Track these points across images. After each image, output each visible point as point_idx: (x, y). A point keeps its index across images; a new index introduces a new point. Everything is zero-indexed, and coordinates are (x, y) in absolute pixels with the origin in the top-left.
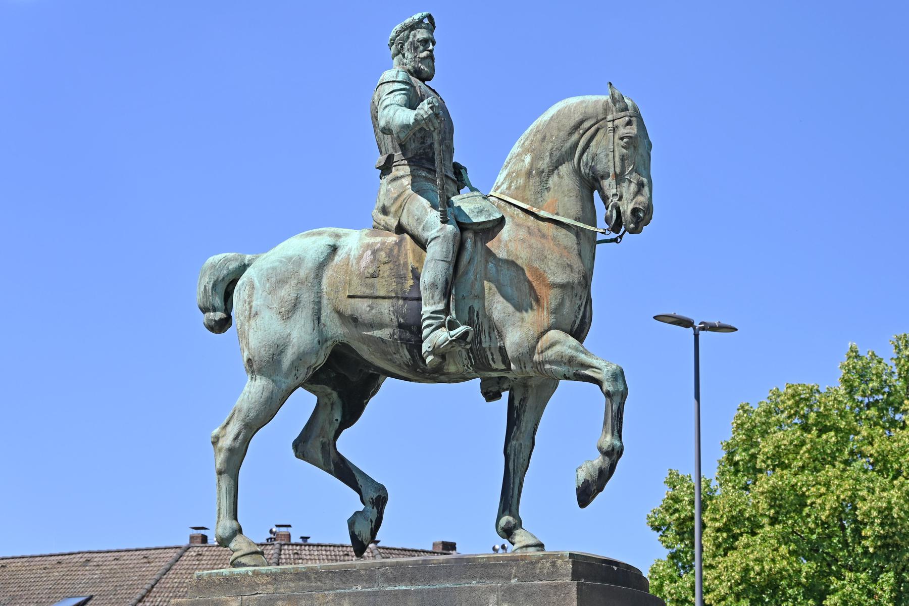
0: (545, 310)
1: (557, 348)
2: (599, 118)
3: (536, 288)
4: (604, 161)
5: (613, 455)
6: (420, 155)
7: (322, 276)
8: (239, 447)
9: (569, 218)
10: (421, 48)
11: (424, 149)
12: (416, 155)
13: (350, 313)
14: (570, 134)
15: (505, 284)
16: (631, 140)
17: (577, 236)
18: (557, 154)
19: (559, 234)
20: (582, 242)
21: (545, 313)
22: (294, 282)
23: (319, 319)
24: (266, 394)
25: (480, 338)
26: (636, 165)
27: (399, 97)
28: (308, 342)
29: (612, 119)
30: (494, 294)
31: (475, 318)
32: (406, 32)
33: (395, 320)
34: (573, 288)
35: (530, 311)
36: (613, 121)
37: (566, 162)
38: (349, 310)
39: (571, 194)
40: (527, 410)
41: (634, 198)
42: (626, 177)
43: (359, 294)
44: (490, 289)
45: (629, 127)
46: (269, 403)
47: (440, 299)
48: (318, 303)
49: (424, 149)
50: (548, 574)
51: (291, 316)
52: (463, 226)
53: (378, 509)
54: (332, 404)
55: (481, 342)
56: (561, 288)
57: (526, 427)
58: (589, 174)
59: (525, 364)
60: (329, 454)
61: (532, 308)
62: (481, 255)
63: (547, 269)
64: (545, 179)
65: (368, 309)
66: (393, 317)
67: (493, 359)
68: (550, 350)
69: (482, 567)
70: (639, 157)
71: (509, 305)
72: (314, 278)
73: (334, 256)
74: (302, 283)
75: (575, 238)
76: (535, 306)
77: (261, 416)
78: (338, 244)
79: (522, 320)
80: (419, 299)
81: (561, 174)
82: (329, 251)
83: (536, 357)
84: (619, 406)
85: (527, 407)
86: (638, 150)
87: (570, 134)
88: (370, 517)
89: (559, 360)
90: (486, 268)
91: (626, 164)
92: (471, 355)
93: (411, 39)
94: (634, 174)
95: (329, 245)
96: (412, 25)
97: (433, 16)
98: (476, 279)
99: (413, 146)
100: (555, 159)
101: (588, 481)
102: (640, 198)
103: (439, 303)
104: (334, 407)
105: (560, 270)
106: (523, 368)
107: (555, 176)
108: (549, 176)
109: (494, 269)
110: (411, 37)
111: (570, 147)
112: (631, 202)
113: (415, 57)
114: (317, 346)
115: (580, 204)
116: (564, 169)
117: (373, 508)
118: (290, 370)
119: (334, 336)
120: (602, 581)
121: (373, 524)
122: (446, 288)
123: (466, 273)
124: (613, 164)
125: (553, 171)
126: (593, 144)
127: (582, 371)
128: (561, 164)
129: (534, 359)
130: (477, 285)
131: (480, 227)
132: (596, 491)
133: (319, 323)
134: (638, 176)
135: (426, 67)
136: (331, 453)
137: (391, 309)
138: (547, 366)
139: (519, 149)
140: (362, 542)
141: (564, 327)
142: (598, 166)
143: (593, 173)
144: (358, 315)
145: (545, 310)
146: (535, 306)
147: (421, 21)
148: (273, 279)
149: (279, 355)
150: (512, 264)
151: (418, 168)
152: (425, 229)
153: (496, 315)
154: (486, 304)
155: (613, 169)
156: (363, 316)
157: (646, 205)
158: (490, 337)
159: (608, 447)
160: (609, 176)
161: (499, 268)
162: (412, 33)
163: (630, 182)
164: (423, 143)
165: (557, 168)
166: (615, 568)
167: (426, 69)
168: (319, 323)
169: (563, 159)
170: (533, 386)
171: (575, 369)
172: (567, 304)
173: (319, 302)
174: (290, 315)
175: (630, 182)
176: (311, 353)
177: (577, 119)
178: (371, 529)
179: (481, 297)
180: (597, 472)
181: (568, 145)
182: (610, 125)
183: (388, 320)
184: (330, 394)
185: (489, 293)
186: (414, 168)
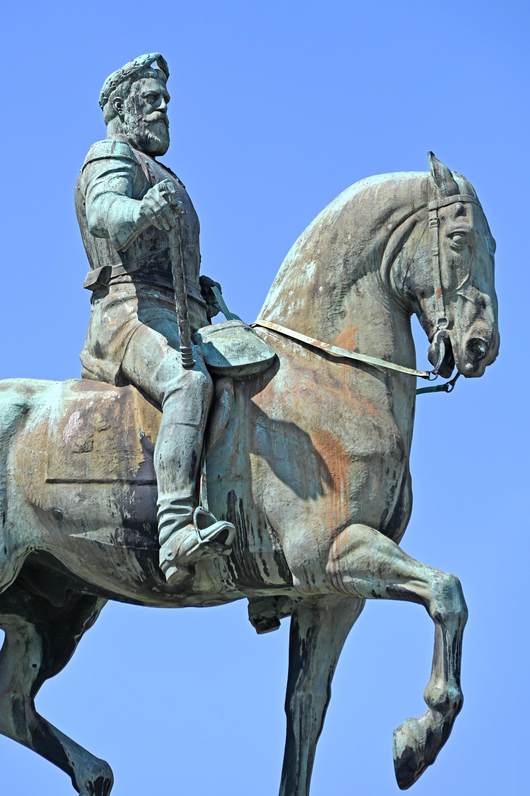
0: (342, 494)
1: (361, 552)
2: (416, 206)
3: (327, 462)
4: (425, 270)
5: (448, 709)
6: (150, 267)
9: (375, 355)
10: (149, 106)
11: (155, 259)
12: (144, 267)
13: (51, 506)
14: (374, 231)
16: (464, 238)
17: (388, 383)
18: (354, 261)
19: (361, 381)
21: (342, 500)
26: (472, 274)
27: (117, 181)
30: (265, 473)
31: (238, 509)
32: (126, 83)
33: (118, 514)
34: (382, 461)
35: (319, 497)
36: (437, 209)
37: (369, 273)
38: (49, 501)
39: (377, 321)
40: (318, 644)
41: (471, 324)
42: (459, 293)
43: (63, 477)
44: (259, 465)
45: (461, 218)
47: (184, 482)
54: (27, 643)
56: (365, 461)
57: (318, 670)
58: (402, 290)
59: (313, 576)
60: (24, 717)
61: (323, 494)
63: (343, 433)
64: (337, 299)
65: (77, 499)
67: (265, 570)
70: (478, 262)
75: (384, 385)
76: (327, 490)
78: (30, 402)
79: (308, 510)
81: (361, 290)
82: (17, 414)
83: (330, 566)
84: (456, 635)
86: (475, 252)
87: (374, 231)
89: (365, 568)
90: (252, 434)
91: (458, 274)
92: (232, 564)
93: (132, 94)
94: (470, 288)
95: (17, 405)
96: (135, 73)
99: (139, 253)
101: (411, 749)
103: (182, 488)
104: (31, 646)
105: (362, 434)
106: (311, 583)
108: (343, 294)
109: (264, 436)
110: (133, 90)
111: (374, 251)
112: (467, 331)
115: (391, 335)
123: (222, 442)
124: (437, 274)
125: (349, 286)
126: (408, 244)
127: (399, 585)
128: (361, 276)
129: (327, 568)
130: (240, 458)
131: (242, 373)
132: (423, 764)
133: (4, 522)
134: (476, 292)
135: (156, 135)
138: (347, 579)
141: (370, 519)
142: (417, 277)
143: (409, 288)
144: (63, 509)
145: (342, 494)
146: (327, 490)
147: (147, 66)
151: (148, 287)
152: (160, 378)
154: (254, 488)
155: (439, 282)
156: (71, 510)
157: (489, 334)
158: (260, 537)
159: (441, 698)
160: (432, 292)
161: (272, 434)
162: (135, 84)
163: (465, 300)
164: (154, 248)
165: (355, 281)
169: (364, 268)
170: (327, 608)
172: (375, 485)
175: (465, 300)
177: (383, 208)
180: (425, 736)
181: (371, 246)
182: (433, 215)
183: (108, 515)
186: (141, 286)
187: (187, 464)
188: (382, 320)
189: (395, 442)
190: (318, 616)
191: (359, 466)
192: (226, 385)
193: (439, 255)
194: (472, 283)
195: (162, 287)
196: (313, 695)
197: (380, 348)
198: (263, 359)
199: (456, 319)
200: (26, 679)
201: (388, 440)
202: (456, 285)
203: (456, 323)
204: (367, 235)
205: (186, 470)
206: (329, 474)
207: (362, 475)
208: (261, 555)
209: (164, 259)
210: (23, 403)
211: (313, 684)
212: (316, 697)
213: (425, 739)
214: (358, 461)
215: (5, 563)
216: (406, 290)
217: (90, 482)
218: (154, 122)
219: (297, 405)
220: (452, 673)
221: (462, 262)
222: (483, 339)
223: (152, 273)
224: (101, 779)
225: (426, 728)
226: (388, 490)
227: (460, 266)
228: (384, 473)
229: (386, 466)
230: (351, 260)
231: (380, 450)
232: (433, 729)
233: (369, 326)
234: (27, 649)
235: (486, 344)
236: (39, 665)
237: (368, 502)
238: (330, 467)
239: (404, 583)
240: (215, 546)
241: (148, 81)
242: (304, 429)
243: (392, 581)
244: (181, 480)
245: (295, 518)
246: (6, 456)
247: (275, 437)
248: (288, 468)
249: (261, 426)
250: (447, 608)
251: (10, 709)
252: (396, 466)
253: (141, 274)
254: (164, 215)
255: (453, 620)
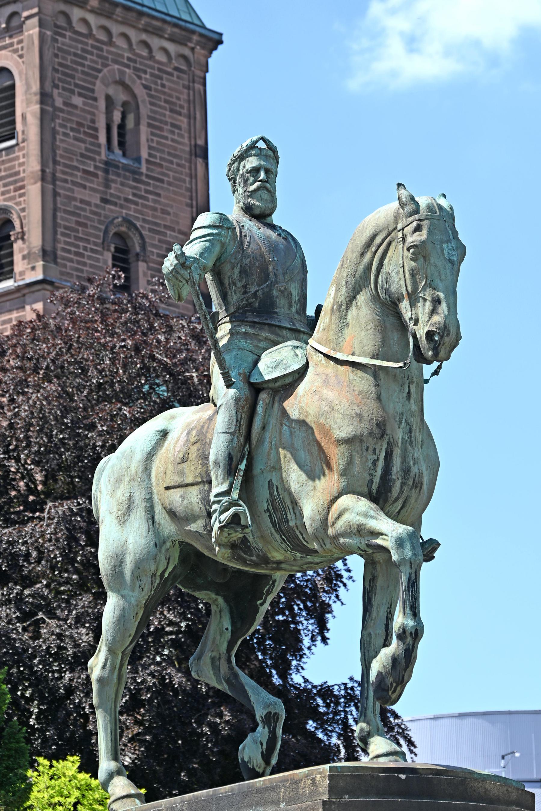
0: (335, 472)
1: (346, 517)
2: (390, 229)
3: (324, 448)
5: (406, 638)
7: (151, 468)
8: (108, 677)
9: (365, 356)
10: (252, 179)
11: (247, 300)
12: (238, 308)
14: (363, 254)
15: (299, 448)
16: (417, 250)
17: (375, 376)
20: (382, 383)
21: (336, 477)
22: (127, 479)
23: (153, 518)
24: (117, 612)
25: (286, 516)
26: (429, 278)
27: (198, 245)
28: (143, 546)
29: (401, 227)
30: (289, 462)
31: (276, 494)
34: (361, 441)
35: (322, 477)
36: (403, 229)
37: (363, 289)
40: (377, 591)
41: (430, 318)
42: (420, 295)
43: (172, 484)
44: (285, 457)
45: (417, 233)
46: (122, 623)
47: (224, 479)
48: (150, 500)
49: (247, 300)
50: (310, 793)
51: (127, 519)
52: (258, 386)
53: (269, 728)
55: (288, 521)
56: (347, 444)
57: (378, 612)
59: (323, 540)
60: (219, 670)
61: (324, 474)
62: (277, 418)
63: (333, 423)
64: (344, 313)
65: (181, 500)
66: (201, 506)
67: (304, 538)
68: (340, 520)
69: (257, 792)
70: (432, 268)
71: (301, 473)
72: (143, 472)
73: (163, 443)
74: (134, 479)
75: (372, 379)
76: (326, 471)
77: (117, 639)
79: (315, 488)
80: (210, 482)
81: (359, 304)
82: (158, 437)
83: (331, 531)
84: (410, 577)
85: (378, 588)
86: (429, 260)
87: (363, 254)
88: (260, 739)
89: (349, 531)
93: (241, 172)
94: (428, 289)
96: (241, 154)
97: (268, 137)
98: (271, 448)
99: (235, 298)
100: (350, 287)
101: (382, 673)
102: (436, 318)
103: (222, 483)
104: (223, 614)
105: (346, 422)
106: (324, 546)
107: (354, 307)
108: (347, 309)
109: (288, 433)
110: (241, 168)
111: (364, 270)
112: (427, 325)
113: (245, 191)
114: (155, 550)
115: (380, 336)
116: (362, 298)
117: (264, 728)
118: (132, 580)
119: (170, 535)
120: (378, 795)
121: (264, 747)
122: (230, 464)
123: (260, 441)
124: (404, 282)
125: (351, 302)
126: (386, 261)
127: (374, 541)
128: (358, 293)
130: (273, 453)
131: (278, 384)
132: (394, 685)
134: (433, 292)
135: (258, 201)
136: (221, 669)
137: (199, 497)
138: (342, 540)
139: (447, 267)
140: (254, 769)
141: (359, 489)
142: (392, 287)
143: (389, 297)
145: (335, 472)
146: (326, 471)
148: (112, 480)
149: (120, 566)
150: (303, 423)
151: (240, 323)
153: (294, 487)
154: (284, 476)
157: (442, 325)
158: (295, 513)
159: (399, 630)
160: (403, 298)
161: (293, 430)
162: (242, 163)
164: (245, 292)
165: (354, 297)
166: (403, 776)
167: (257, 203)
168: (153, 523)
169: (360, 286)
170: (381, 561)
171: (366, 538)
172: (357, 461)
173: (151, 499)
174: (126, 518)
175: (425, 300)
176: (147, 559)
177: (368, 235)
178: (262, 753)
179: (277, 468)
180: (390, 661)
181: (361, 268)
182: (400, 234)
183: (198, 509)
184: (216, 600)
185: (284, 462)
186: (235, 324)
187: (224, 464)
188: (373, 326)
189: (374, 424)
190: (375, 568)
191: (343, 448)
192: (263, 396)
193: (403, 266)
194: (431, 285)
195: (251, 322)
196: (372, 633)
197: (369, 349)
198: (291, 371)
199: (420, 316)
200: (222, 640)
201: (368, 423)
202: (417, 289)
203: (420, 319)
204: (358, 258)
205: (224, 469)
206: (326, 457)
207: (347, 455)
208: (297, 527)
209: (254, 300)
210: (163, 428)
211: (374, 624)
212: (376, 634)
213: (391, 664)
214: (342, 444)
215: (156, 555)
216: (388, 299)
217: (187, 485)
218: (255, 191)
219: (307, 404)
220: (408, 608)
221: (419, 270)
222: (435, 330)
223: (245, 312)
224: (269, 713)
225: (391, 655)
226: (370, 464)
227: (418, 273)
228: (364, 450)
229: (365, 445)
230: (350, 280)
231: (359, 433)
232: (396, 655)
233: (363, 332)
234: (221, 617)
235: (439, 333)
236: (230, 628)
237: (354, 476)
238: (327, 451)
239: (377, 538)
240: (233, 527)
241: (250, 159)
242: (309, 423)
243: (369, 538)
244: (221, 478)
245: (308, 495)
246: (150, 472)
247: (295, 432)
248: (303, 456)
249: (286, 425)
250: (399, 556)
251: (210, 665)
252: (376, 443)
253: (237, 314)
254: (177, 273)
255: (405, 565)
